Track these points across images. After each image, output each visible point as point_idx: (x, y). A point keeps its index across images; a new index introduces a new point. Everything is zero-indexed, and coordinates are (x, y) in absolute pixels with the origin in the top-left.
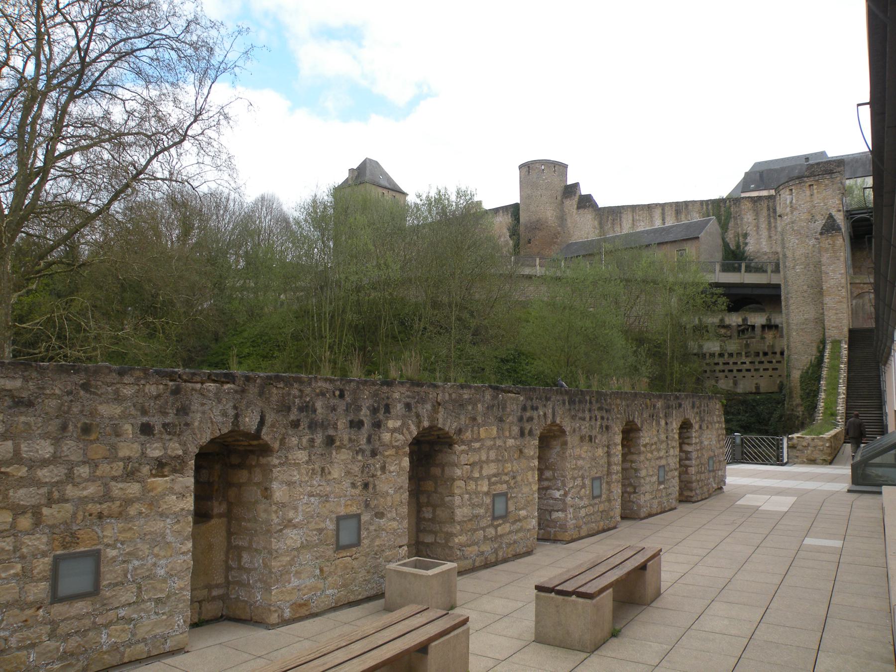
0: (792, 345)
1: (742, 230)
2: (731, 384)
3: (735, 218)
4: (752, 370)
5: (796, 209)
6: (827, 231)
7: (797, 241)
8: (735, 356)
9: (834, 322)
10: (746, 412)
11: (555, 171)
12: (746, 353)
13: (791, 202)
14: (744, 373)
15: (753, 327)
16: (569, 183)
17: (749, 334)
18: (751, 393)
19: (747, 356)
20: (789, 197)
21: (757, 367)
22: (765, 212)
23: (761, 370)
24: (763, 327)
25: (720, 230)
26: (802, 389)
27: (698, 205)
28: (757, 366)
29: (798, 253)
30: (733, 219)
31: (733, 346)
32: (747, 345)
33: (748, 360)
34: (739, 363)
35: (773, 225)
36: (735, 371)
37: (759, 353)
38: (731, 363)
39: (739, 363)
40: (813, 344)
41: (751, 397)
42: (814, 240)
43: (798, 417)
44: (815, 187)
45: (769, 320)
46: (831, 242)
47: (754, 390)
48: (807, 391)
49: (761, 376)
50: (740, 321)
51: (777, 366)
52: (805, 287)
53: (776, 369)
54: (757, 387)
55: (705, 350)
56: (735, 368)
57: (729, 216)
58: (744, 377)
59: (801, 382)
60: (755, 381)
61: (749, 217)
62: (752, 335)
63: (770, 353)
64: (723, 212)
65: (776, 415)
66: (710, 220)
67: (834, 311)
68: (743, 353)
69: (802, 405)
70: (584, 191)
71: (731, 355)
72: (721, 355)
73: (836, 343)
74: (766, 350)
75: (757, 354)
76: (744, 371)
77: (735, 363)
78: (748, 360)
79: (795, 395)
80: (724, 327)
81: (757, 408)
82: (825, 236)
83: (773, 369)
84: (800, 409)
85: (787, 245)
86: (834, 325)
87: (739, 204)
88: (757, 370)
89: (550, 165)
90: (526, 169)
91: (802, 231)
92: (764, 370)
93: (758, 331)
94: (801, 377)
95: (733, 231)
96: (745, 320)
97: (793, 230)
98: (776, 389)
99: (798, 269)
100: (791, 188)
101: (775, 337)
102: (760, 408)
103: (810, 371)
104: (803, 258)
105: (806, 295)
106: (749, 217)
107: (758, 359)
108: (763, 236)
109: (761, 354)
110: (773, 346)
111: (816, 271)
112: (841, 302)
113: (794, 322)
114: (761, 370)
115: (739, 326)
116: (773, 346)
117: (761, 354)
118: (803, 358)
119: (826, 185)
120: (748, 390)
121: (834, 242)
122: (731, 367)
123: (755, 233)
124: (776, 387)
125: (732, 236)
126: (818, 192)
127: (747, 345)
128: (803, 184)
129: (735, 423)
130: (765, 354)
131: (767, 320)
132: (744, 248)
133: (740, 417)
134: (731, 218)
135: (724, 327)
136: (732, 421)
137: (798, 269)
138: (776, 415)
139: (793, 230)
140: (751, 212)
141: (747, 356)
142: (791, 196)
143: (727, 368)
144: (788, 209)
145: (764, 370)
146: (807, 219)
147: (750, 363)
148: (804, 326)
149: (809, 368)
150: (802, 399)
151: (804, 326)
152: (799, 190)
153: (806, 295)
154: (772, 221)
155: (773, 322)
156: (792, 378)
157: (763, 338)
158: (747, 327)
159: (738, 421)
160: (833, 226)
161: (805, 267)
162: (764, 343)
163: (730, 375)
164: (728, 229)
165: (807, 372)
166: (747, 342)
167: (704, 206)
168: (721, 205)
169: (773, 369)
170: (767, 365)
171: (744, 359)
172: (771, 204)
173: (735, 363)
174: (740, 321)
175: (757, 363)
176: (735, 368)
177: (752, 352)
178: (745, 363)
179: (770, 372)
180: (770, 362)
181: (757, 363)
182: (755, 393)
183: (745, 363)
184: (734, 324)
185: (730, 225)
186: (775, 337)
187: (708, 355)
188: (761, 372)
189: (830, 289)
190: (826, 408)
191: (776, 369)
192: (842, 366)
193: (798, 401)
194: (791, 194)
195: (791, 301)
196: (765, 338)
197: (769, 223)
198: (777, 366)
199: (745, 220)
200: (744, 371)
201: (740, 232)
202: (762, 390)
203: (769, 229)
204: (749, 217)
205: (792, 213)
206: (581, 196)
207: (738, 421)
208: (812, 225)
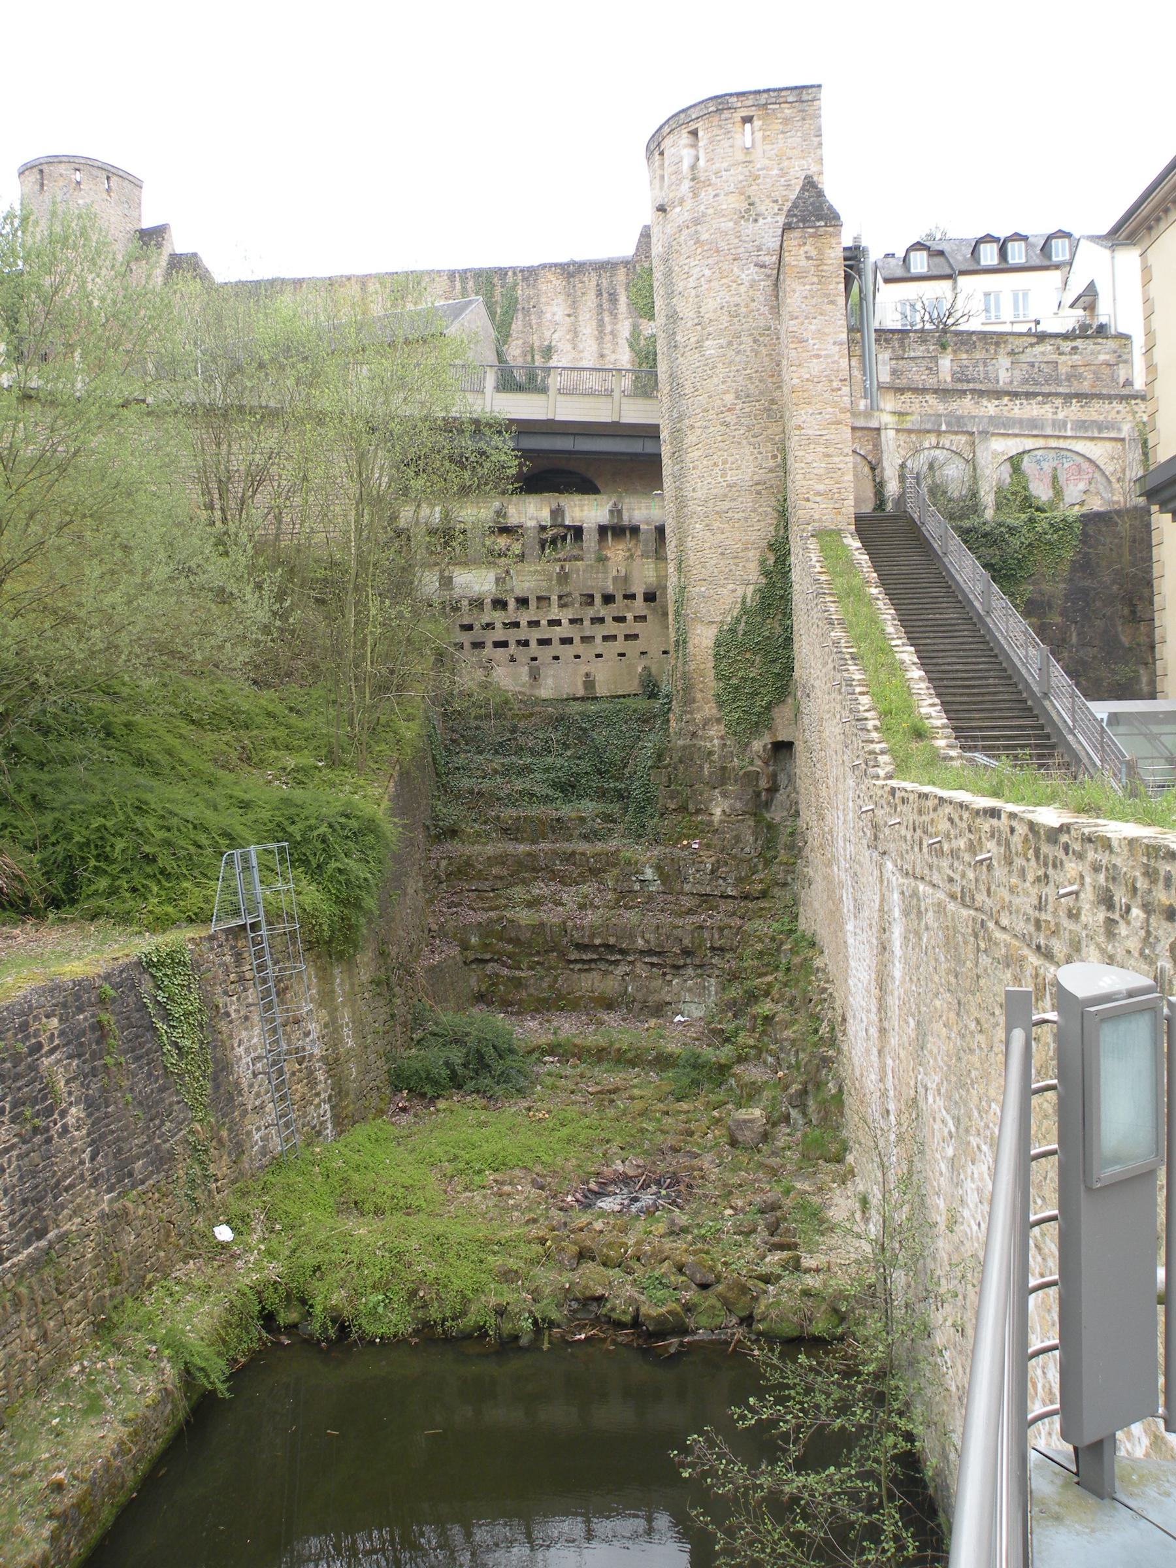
0: (692, 558)
1: (541, 338)
2: (525, 678)
3: (527, 312)
4: (577, 640)
5: (708, 183)
6: (804, 220)
7: (707, 272)
8: (533, 603)
9: (820, 478)
10: (566, 746)
11: (108, 190)
12: (560, 597)
13: (693, 167)
14: (556, 648)
15: (578, 532)
16: (146, 224)
17: (569, 548)
18: (575, 699)
19: (562, 606)
20: (687, 155)
21: (587, 634)
22: (590, 300)
23: (599, 640)
24: (603, 530)
25: (493, 333)
26: (720, 677)
27: (442, 284)
28: (588, 629)
29: (710, 306)
30: (520, 315)
31: (526, 581)
32: (563, 577)
33: (565, 616)
34: (544, 622)
35: (608, 328)
36: (533, 644)
37: (592, 596)
38: (524, 623)
39: (544, 622)
40: (751, 554)
41: (577, 707)
42: (753, 269)
43: (711, 753)
44: (757, 123)
45: (616, 512)
46: (813, 253)
47: (581, 692)
48: (734, 681)
49: (599, 656)
50: (545, 516)
51: (638, 628)
52: (729, 398)
53: (635, 637)
54: (589, 683)
55: (457, 592)
56: (534, 635)
57: (512, 306)
58: (556, 658)
59: (718, 657)
60: (584, 669)
61: (555, 309)
62: (575, 552)
63: (619, 598)
64: (498, 298)
65: (648, 746)
66: (470, 302)
67: (821, 449)
68: (554, 598)
69: (718, 721)
70: (180, 243)
71: (523, 602)
72: (500, 604)
73: (827, 536)
74: (610, 589)
75: (589, 599)
76: (556, 642)
77: (534, 624)
78: (565, 616)
79: (699, 696)
80: (505, 530)
81: (594, 735)
82: (796, 234)
83: (627, 637)
84: (716, 731)
85: (680, 286)
86: (821, 487)
87: (536, 280)
88: (586, 640)
89: (95, 172)
90: (34, 176)
91: (723, 245)
92: (606, 638)
93: (590, 540)
94: (718, 644)
95: (520, 342)
96: (557, 513)
97: (697, 241)
98: (634, 686)
99: (711, 348)
100: (693, 126)
101: (631, 556)
102: (599, 736)
103: (742, 627)
104: (726, 318)
105: (730, 418)
106: (555, 310)
107: (591, 612)
108: (586, 354)
109: (598, 600)
110: (626, 579)
111: (757, 353)
112: (839, 423)
113: (699, 494)
114: (599, 640)
115: (543, 528)
116: (626, 579)
117: (598, 600)
118: (724, 591)
119: (786, 121)
120: (566, 691)
121: (820, 252)
122: (523, 633)
123: (569, 347)
124: (636, 682)
125: (517, 352)
126: (765, 138)
127: (563, 577)
128: (726, 114)
129: (539, 776)
130: (608, 599)
131: (611, 511)
132: (543, 381)
133: (550, 760)
134: (516, 310)
135: (505, 530)
136: (532, 771)
137: (711, 348)
138: (648, 746)
139: (697, 241)
140: (562, 298)
141: (562, 606)
142: (692, 152)
143: (512, 636)
144: (686, 185)
145: (606, 638)
146: (735, 211)
147: (572, 621)
148: (726, 505)
149: (738, 620)
150: (721, 705)
151: (726, 505)
152: (716, 131)
153: (730, 418)
154: (607, 319)
155: (625, 520)
156: (690, 648)
157: (602, 559)
158: (562, 531)
159: (546, 770)
160: (820, 208)
161: (730, 343)
162: (606, 572)
163: (523, 655)
164: (508, 335)
165: (733, 631)
166: (562, 567)
167: (458, 285)
168: (496, 280)
169: (627, 637)
170: (611, 628)
171: (555, 613)
172: (605, 283)
173: (534, 624)
174: (545, 516)
175: (587, 623)
176: (534, 635)
177: (576, 594)
178: (558, 623)
179: (620, 645)
180: (620, 619)
181: (587, 623)
182: (582, 699)
183: (558, 623)
184: (531, 524)
185: (514, 326)
186: (631, 556)
187: (465, 603)
188: (599, 646)
189: (810, 386)
190: (885, 714)
191: (635, 637)
192: (874, 591)
193: (709, 709)
194: (694, 146)
195: (691, 439)
196: (606, 559)
197: (601, 324)
198: (638, 628)
199: (548, 316)
200: (556, 642)
201: (536, 344)
202: (601, 690)
203: (600, 338)
204: (555, 309)
205: (695, 195)
206: (173, 256)
207: (546, 770)
208: (749, 228)
